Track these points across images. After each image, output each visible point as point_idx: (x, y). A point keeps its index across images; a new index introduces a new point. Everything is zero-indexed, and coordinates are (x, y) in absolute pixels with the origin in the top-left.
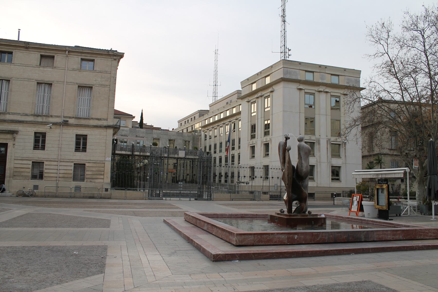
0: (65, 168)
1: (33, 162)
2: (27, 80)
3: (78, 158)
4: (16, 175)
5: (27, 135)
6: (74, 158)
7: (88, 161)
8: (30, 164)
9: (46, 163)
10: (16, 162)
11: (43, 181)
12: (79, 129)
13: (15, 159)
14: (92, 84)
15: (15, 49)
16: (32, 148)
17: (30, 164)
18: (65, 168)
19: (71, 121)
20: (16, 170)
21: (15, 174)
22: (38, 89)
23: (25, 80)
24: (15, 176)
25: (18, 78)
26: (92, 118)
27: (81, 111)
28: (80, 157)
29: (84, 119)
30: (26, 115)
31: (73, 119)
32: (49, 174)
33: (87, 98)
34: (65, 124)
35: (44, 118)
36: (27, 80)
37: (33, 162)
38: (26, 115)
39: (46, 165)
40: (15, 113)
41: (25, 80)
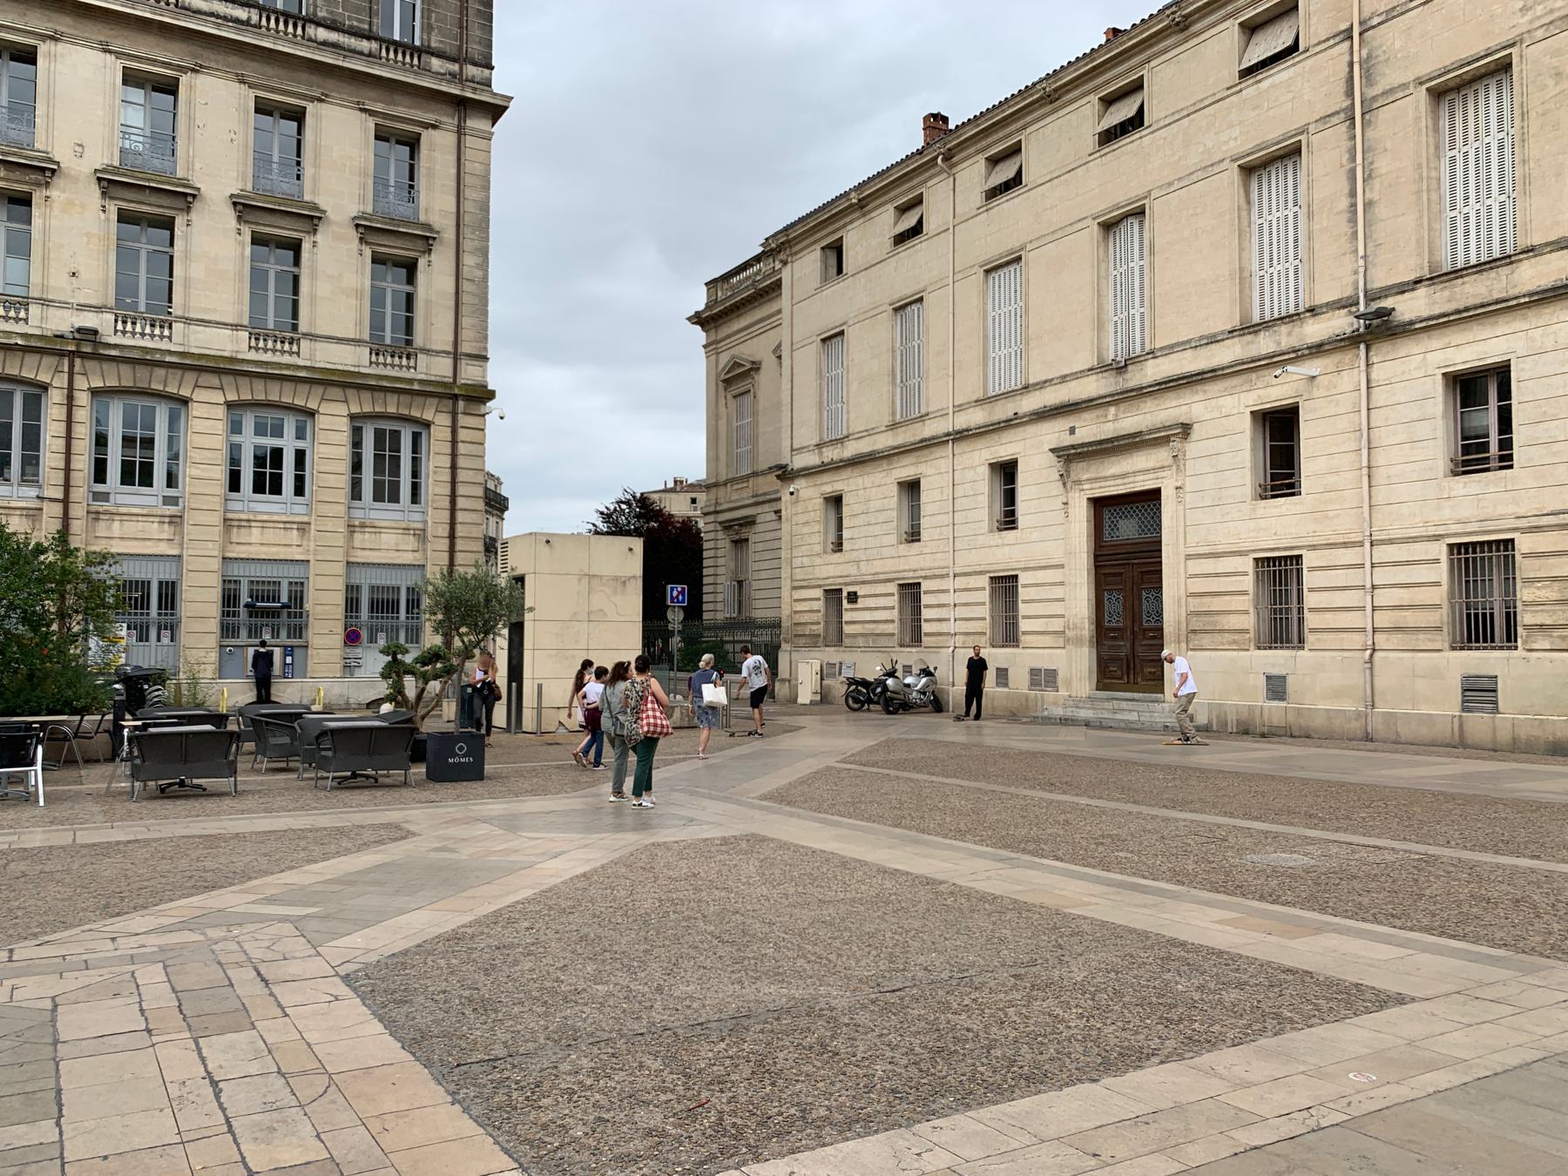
0: (1402, 575)
1: (1451, 546)
2: (1200, 175)
3: (928, 564)
4: (1200, 631)
5: (1225, 427)
6: (1447, 513)
7: (1523, 523)
8: (1245, 574)
9: (1309, 559)
10: (1196, 567)
11: (1520, 653)
12: (1455, 336)
13: (1188, 557)
14: (1017, 245)
15: (1024, 128)
16: (1442, 464)
17: (1245, 574)
18: (1402, 575)
19: (1408, 307)
20: (1195, 604)
21: (1196, 624)
22: (1255, 196)
23: (1194, 178)
24: (1194, 631)
25: (1170, 184)
26: (1530, 250)
27: (1467, 233)
28: (1482, 505)
29: (1491, 264)
30: (1213, 340)
31: (1422, 291)
32: (1329, 615)
33: (1135, 265)
34: (1379, 329)
35: (1284, 329)
36: (1200, 175)
37: (1451, 546)
38: (1213, 340)
39: (1312, 569)
40: (1172, 346)
41: (1194, 178)
